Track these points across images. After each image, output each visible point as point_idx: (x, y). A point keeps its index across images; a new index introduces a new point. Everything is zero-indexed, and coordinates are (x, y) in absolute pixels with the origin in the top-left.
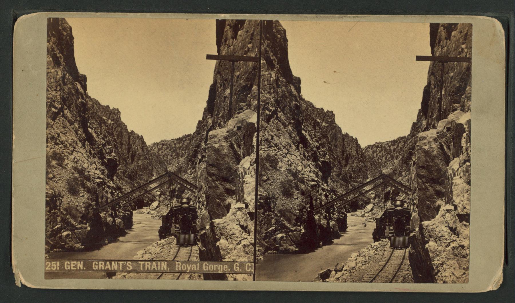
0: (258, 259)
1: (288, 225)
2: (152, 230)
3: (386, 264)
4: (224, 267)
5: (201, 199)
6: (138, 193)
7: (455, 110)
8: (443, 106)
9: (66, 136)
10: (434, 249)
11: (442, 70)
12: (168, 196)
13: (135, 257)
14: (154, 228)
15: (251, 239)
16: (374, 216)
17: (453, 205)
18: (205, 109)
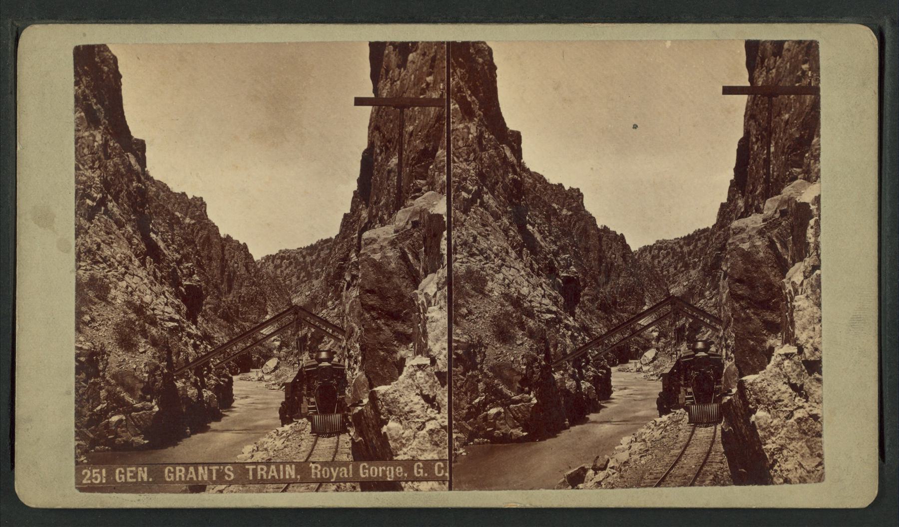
0: (456, 454)
1: (508, 392)
2: (267, 409)
3: (683, 452)
4: (397, 470)
5: (351, 352)
6: (241, 345)
7: (795, 178)
8: (773, 172)
9: (111, 247)
10: (765, 424)
11: (769, 110)
12: (294, 348)
13: (239, 456)
14: (272, 406)
15: (442, 419)
16: (659, 371)
17: (797, 345)
18: (355, 192)
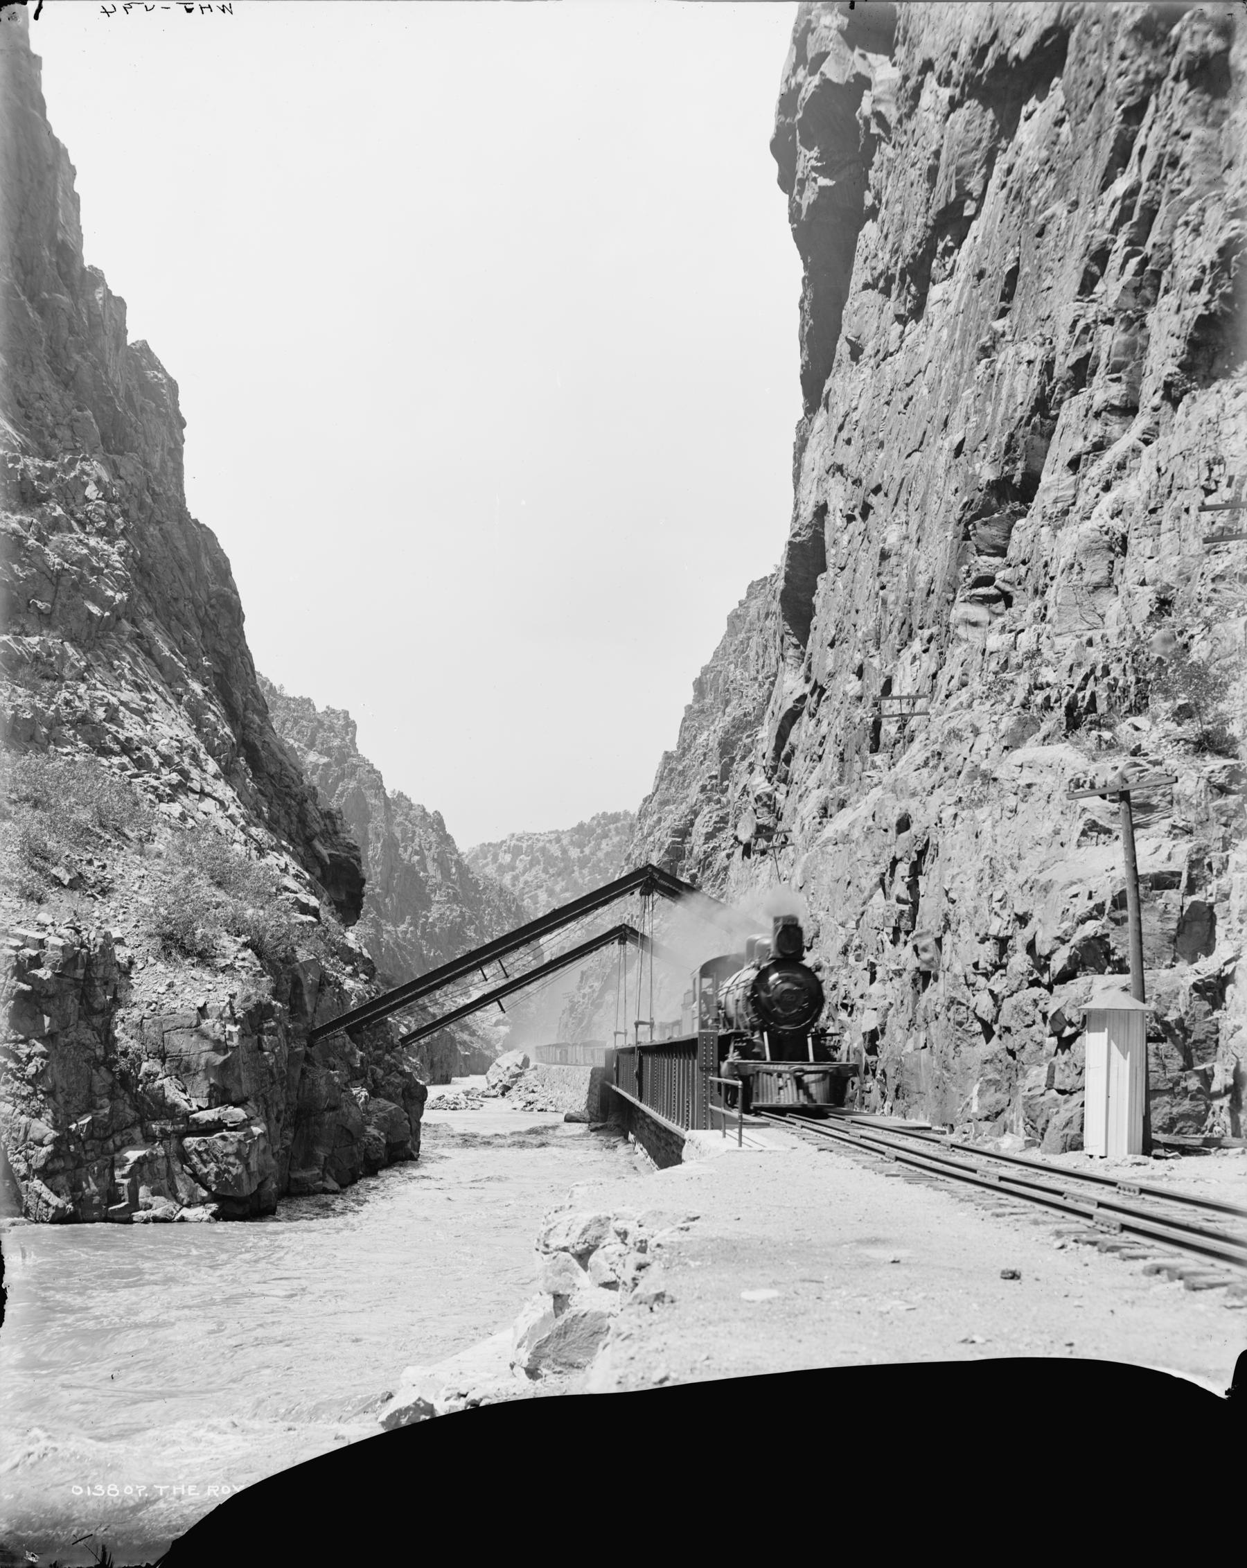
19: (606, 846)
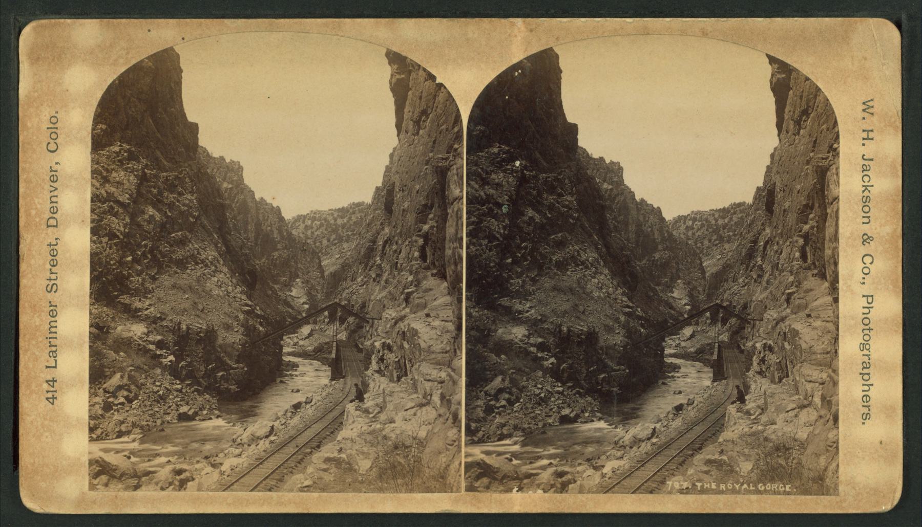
12: (707, 318)
19: (735, 219)
